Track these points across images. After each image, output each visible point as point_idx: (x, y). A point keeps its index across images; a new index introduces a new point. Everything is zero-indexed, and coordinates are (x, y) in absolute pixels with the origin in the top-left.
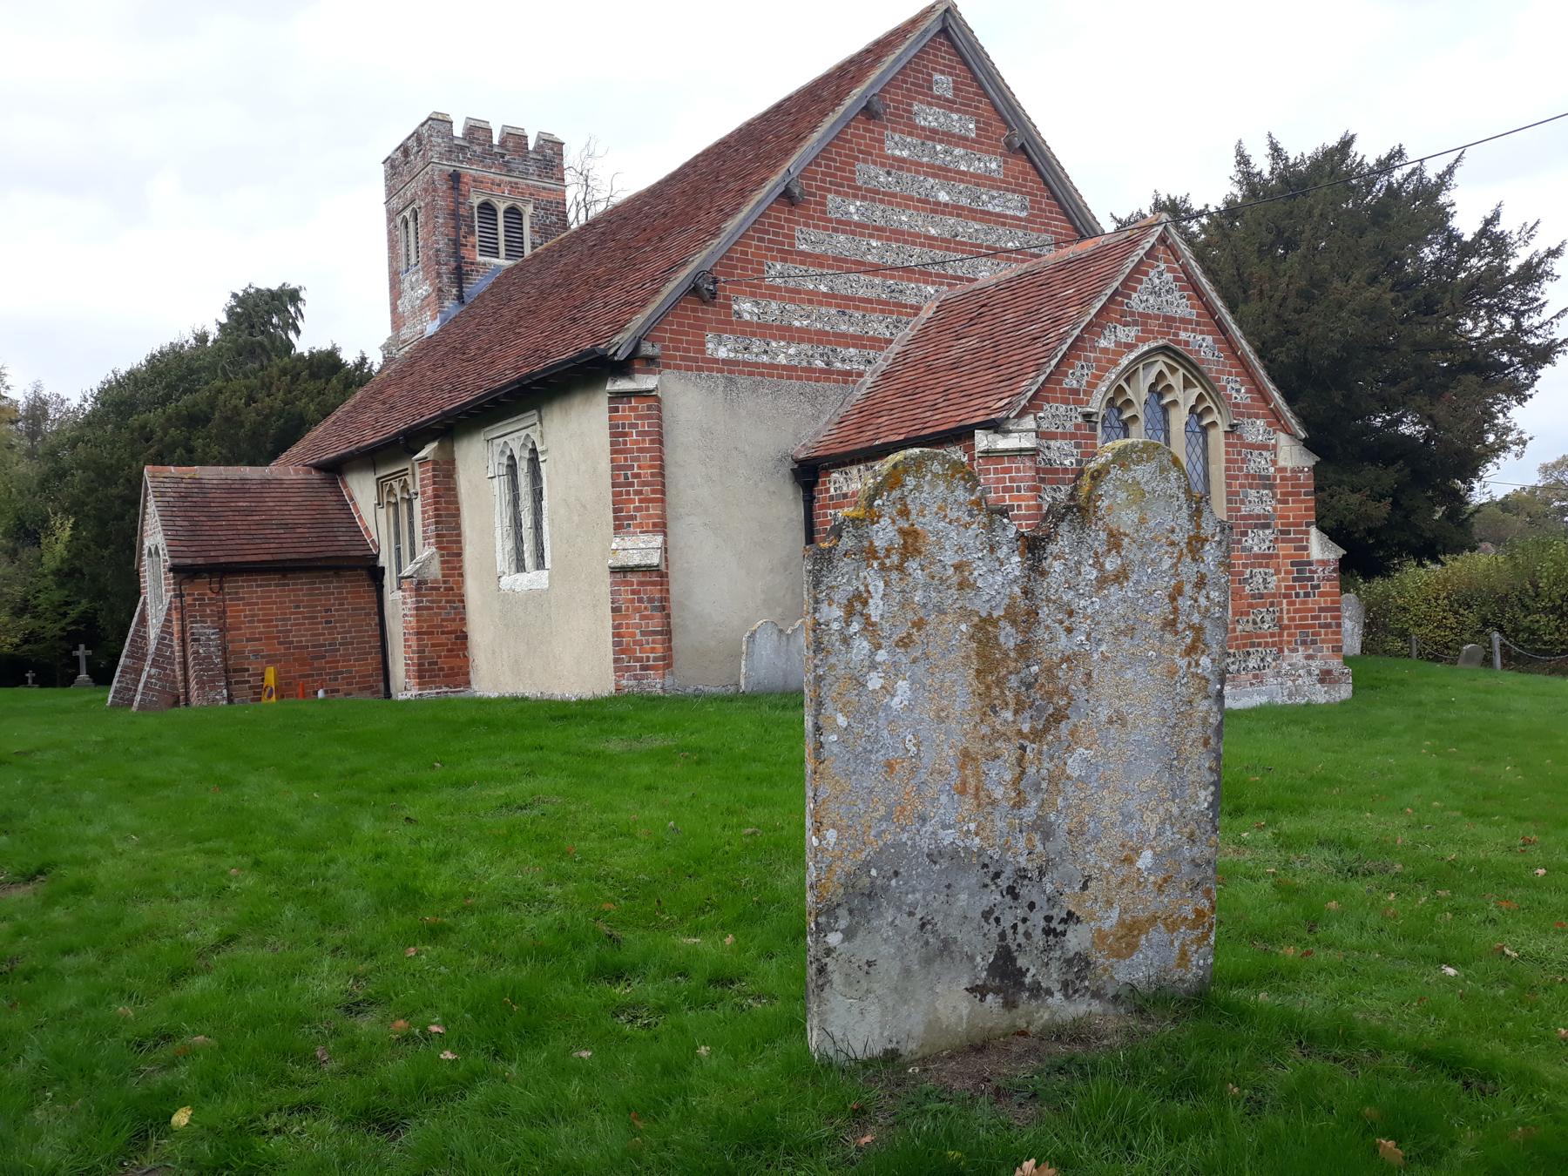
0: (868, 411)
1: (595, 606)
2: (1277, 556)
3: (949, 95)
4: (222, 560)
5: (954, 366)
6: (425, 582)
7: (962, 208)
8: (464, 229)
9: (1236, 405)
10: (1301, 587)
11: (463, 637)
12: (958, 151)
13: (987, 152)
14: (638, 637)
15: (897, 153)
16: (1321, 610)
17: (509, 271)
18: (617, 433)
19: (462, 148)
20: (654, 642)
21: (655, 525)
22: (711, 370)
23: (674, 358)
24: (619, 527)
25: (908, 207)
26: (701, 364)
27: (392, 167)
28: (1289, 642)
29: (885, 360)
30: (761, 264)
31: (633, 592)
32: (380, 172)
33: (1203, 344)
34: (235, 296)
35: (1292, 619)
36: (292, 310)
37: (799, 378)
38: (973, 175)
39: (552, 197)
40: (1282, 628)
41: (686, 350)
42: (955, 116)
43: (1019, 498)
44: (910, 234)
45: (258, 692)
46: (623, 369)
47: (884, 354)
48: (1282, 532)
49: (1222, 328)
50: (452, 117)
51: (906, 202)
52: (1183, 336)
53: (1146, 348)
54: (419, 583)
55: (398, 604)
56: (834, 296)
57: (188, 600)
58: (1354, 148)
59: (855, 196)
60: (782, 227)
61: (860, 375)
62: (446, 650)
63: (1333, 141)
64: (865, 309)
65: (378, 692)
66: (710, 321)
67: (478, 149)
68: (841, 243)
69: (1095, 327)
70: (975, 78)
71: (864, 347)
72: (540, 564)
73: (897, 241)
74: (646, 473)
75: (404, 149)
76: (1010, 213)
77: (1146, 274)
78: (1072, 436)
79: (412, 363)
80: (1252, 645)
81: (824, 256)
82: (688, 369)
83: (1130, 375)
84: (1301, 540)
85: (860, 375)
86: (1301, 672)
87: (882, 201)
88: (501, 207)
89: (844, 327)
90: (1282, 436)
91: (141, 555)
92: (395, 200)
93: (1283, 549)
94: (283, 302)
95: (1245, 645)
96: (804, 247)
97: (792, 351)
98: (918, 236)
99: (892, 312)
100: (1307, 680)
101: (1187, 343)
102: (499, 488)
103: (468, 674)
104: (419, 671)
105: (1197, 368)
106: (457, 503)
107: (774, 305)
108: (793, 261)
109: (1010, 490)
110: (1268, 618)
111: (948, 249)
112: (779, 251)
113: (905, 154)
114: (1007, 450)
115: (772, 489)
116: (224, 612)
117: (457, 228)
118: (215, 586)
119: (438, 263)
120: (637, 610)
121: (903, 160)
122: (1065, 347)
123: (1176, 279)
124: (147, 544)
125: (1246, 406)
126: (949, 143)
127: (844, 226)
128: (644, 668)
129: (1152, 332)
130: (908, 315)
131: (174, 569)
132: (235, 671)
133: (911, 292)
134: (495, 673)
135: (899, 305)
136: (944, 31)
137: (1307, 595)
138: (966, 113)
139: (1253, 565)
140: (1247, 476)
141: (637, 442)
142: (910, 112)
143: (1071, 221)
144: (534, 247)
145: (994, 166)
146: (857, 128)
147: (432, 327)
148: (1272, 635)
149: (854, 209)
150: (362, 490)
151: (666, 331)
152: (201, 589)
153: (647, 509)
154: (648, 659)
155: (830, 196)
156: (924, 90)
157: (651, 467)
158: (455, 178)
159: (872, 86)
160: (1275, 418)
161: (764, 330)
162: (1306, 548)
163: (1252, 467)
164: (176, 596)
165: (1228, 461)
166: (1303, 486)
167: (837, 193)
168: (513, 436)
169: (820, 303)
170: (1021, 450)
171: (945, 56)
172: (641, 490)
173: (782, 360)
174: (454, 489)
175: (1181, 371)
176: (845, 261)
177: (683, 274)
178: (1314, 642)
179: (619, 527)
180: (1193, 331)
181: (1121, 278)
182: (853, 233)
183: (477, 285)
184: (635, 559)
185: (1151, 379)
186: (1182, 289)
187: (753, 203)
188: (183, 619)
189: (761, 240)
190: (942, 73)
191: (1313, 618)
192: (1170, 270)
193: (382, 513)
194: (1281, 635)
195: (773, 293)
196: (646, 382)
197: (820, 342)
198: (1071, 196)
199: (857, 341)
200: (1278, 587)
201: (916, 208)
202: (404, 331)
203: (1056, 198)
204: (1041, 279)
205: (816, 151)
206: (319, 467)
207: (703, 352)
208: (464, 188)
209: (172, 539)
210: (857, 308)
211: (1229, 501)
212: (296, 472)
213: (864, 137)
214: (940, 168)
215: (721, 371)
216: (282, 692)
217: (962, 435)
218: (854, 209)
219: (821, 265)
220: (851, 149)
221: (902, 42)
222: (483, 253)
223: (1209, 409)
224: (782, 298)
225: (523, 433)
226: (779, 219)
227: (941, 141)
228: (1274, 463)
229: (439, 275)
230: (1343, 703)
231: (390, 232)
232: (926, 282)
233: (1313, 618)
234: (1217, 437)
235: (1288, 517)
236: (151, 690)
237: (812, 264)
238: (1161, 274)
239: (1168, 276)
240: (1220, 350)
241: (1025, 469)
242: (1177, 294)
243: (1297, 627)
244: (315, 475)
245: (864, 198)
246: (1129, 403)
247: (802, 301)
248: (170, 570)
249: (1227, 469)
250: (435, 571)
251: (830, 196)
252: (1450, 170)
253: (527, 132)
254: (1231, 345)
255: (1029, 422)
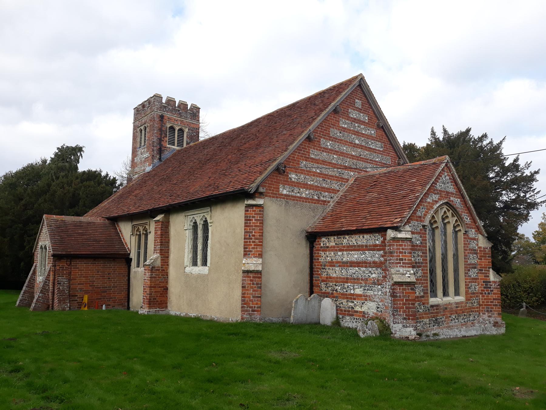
0: (335, 216)
1: (229, 283)
2: (478, 279)
3: (360, 107)
4: (72, 253)
5: (370, 203)
6: (155, 267)
7: (363, 146)
8: (163, 135)
9: (467, 224)
10: (487, 291)
11: (166, 289)
12: (362, 127)
13: (371, 127)
14: (251, 298)
15: (343, 126)
16: (494, 299)
17: (179, 151)
18: (247, 220)
19: (165, 107)
20: (257, 301)
21: (259, 255)
22: (281, 198)
23: (269, 193)
24: (246, 254)
25: (346, 144)
26: (277, 196)
27: (137, 111)
28: (482, 311)
29: (337, 197)
30: (299, 161)
31: (251, 281)
32: (132, 112)
33: (457, 202)
34: (58, 148)
35: (483, 302)
36: (79, 154)
37: (309, 202)
38: (366, 135)
39: (195, 126)
40: (480, 305)
41: (273, 191)
42: (362, 115)
43: (405, 256)
44: (346, 154)
45: (80, 305)
46: (251, 196)
47: (337, 195)
48: (480, 270)
49: (463, 197)
50: (162, 96)
51: (346, 143)
52: (452, 198)
53: (441, 203)
54: (152, 267)
55: (139, 276)
56: (321, 174)
57: (58, 268)
58: (471, 133)
59: (330, 140)
60: (306, 149)
61: (329, 202)
62: (159, 293)
63: (464, 130)
64: (331, 179)
65: (125, 306)
66: (281, 180)
67: (171, 108)
68: (324, 156)
69: (426, 195)
70: (368, 102)
71: (330, 192)
72: (205, 263)
73: (342, 156)
74: (257, 235)
75: (143, 105)
76: (377, 149)
77: (441, 176)
78: (419, 233)
79: (138, 184)
80: (472, 311)
81: (319, 160)
82: (273, 197)
83: (436, 212)
84: (487, 273)
85: (329, 202)
86: (487, 322)
87: (338, 142)
88: (177, 128)
89: (324, 185)
90: (480, 235)
91: (36, 247)
92: (137, 122)
93: (481, 276)
94: (77, 151)
95: (469, 312)
96: (313, 156)
97: (307, 192)
98: (349, 155)
99: (339, 181)
100: (489, 325)
101: (453, 201)
102: (188, 235)
103: (167, 303)
104: (149, 302)
105: (456, 210)
106: (169, 237)
107: (302, 176)
108: (309, 161)
109: (402, 253)
110: (476, 302)
111: (358, 160)
112: (305, 157)
113: (346, 126)
114: (401, 238)
115: (298, 242)
116: (71, 273)
117: (161, 134)
118: (68, 263)
119: (153, 146)
120: (252, 287)
121: (345, 128)
122: (418, 201)
123: (450, 179)
124: (40, 244)
125: (469, 224)
126: (359, 123)
127: (326, 150)
128: (253, 311)
129: (442, 197)
130: (345, 182)
131: (54, 255)
132: (72, 296)
133: (346, 174)
134: (179, 304)
135: (342, 178)
136: (360, 85)
137: (489, 293)
138: (365, 113)
139: (471, 282)
140: (470, 249)
141: (254, 223)
142: (348, 112)
143: (396, 153)
144: (187, 144)
145: (373, 132)
146: (331, 116)
147: (148, 169)
148: (477, 308)
149: (329, 144)
150: (126, 230)
151: (267, 183)
152: (63, 264)
153: (257, 248)
154: (255, 307)
155: (322, 139)
156: (352, 105)
157: (259, 233)
158: (162, 117)
159: (337, 102)
160: (478, 229)
161: (299, 185)
162: (488, 276)
163: (471, 246)
164: (53, 266)
165: (464, 244)
166: (487, 254)
167: (324, 138)
168: (198, 216)
169: (317, 176)
170: (407, 238)
171: (360, 94)
172: (254, 242)
173: (304, 195)
174: (168, 232)
175: (451, 211)
176: (325, 162)
177: (275, 164)
178: (491, 311)
179: (246, 254)
180: (455, 197)
181: (435, 178)
182: (329, 152)
183: (166, 155)
184: (252, 268)
185: (442, 214)
186: (451, 182)
187: (298, 140)
188: (55, 275)
189: (299, 153)
190: (358, 99)
191: (491, 302)
192: (448, 175)
193: (133, 238)
194: (480, 308)
195: (302, 172)
196: (260, 202)
197: (316, 190)
198: (397, 144)
199: (329, 190)
200: (479, 290)
201: (349, 145)
202: (136, 169)
203: (391, 144)
204: (399, 174)
205: (319, 123)
206: (108, 219)
207: (279, 191)
208: (165, 121)
209: (54, 244)
210: (329, 179)
211: (465, 258)
212: (100, 220)
213: (333, 120)
214: (356, 132)
215: (284, 198)
216: (90, 305)
217: (382, 230)
218: (329, 144)
219: (318, 163)
220: (329, 123)
221: (347, 88)
222: (169, 144)
223: (459, 225)
224: (305, 174)
225: (202, 215)
226: (305, 146)
227: (357, 123)
228: (477, 245)
229: (153, 150)
230: (503, 335)
231: (134, 133)
232: (351, 171)
233: (491, 302)
234: (461, 235)
235: (482, 265)
236: (39, 302)
237: (315, 163)
238: (445, 176)
239: (448, 177)
240: (462, 204)
241: (407, 246)
242: (450, 184)
243: (485, 305)
244: (107, 221)
245: (332, 141)
246: (436, 222)
247: (311, 175)
248: (52, 256)
249: (464, 247)
250: (159, 263)
251: (322, 139)
252: (501, 143)
253: (188, 103)
254: (465, 203)
255: (407, 228)
